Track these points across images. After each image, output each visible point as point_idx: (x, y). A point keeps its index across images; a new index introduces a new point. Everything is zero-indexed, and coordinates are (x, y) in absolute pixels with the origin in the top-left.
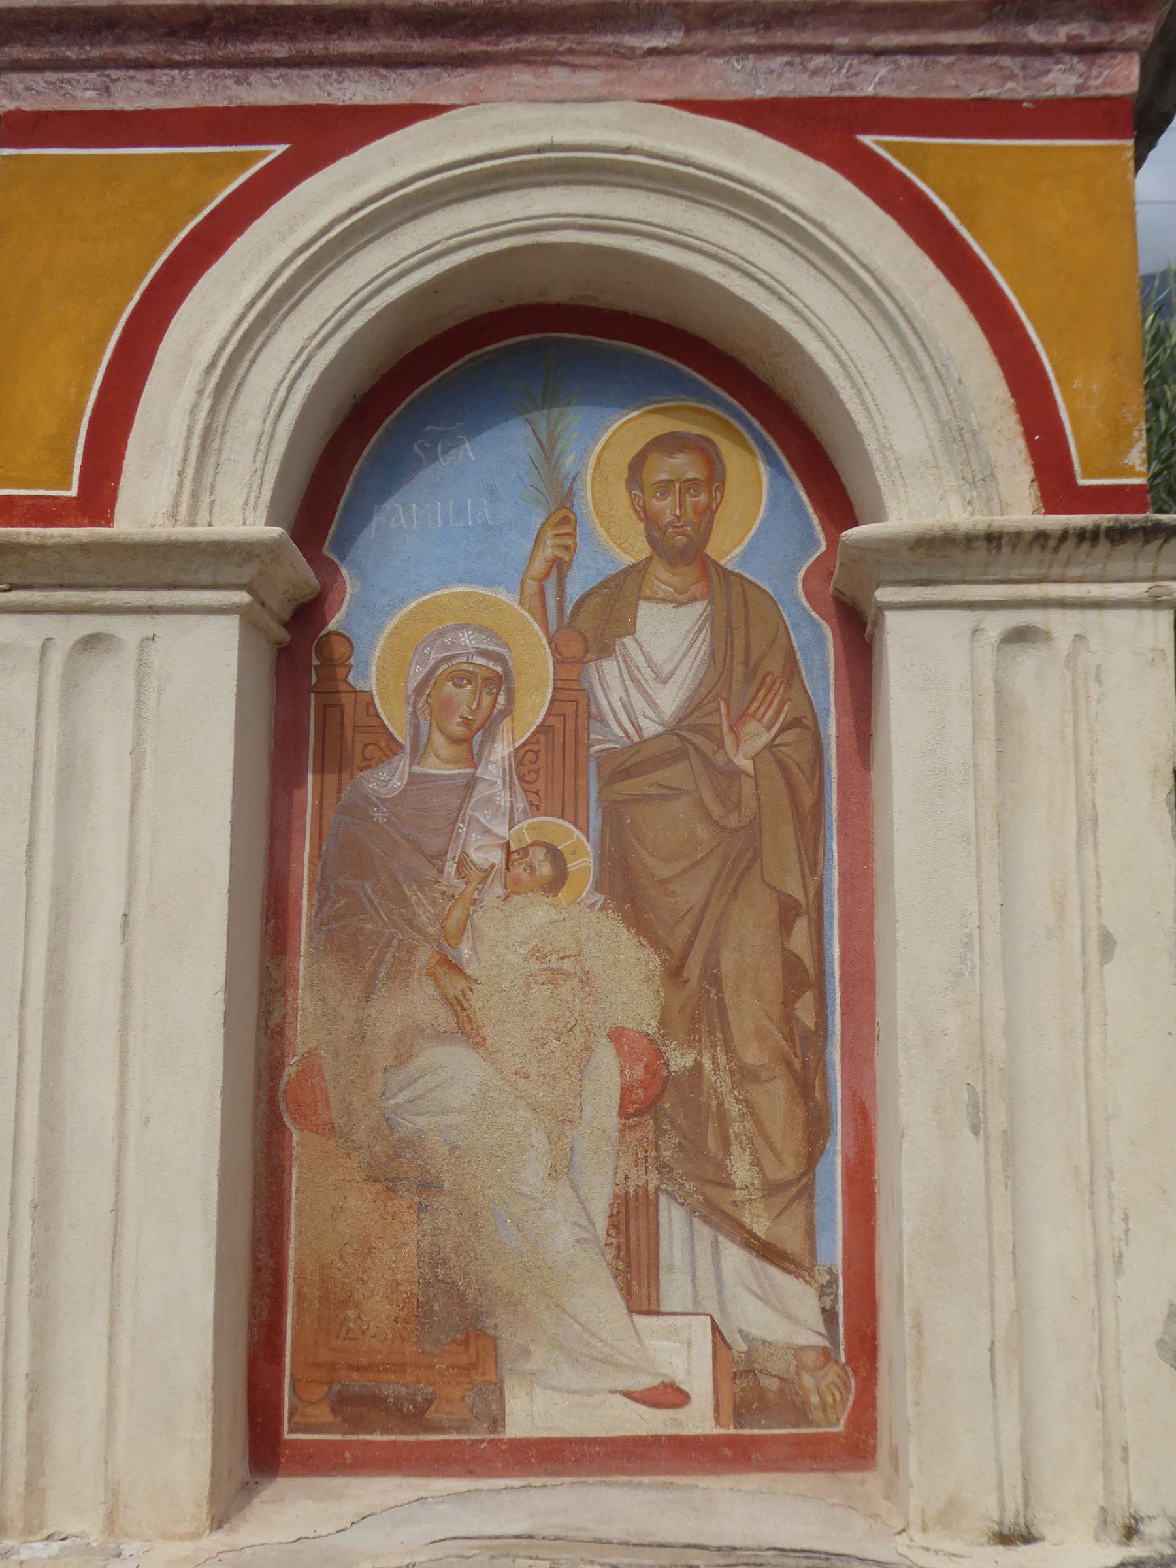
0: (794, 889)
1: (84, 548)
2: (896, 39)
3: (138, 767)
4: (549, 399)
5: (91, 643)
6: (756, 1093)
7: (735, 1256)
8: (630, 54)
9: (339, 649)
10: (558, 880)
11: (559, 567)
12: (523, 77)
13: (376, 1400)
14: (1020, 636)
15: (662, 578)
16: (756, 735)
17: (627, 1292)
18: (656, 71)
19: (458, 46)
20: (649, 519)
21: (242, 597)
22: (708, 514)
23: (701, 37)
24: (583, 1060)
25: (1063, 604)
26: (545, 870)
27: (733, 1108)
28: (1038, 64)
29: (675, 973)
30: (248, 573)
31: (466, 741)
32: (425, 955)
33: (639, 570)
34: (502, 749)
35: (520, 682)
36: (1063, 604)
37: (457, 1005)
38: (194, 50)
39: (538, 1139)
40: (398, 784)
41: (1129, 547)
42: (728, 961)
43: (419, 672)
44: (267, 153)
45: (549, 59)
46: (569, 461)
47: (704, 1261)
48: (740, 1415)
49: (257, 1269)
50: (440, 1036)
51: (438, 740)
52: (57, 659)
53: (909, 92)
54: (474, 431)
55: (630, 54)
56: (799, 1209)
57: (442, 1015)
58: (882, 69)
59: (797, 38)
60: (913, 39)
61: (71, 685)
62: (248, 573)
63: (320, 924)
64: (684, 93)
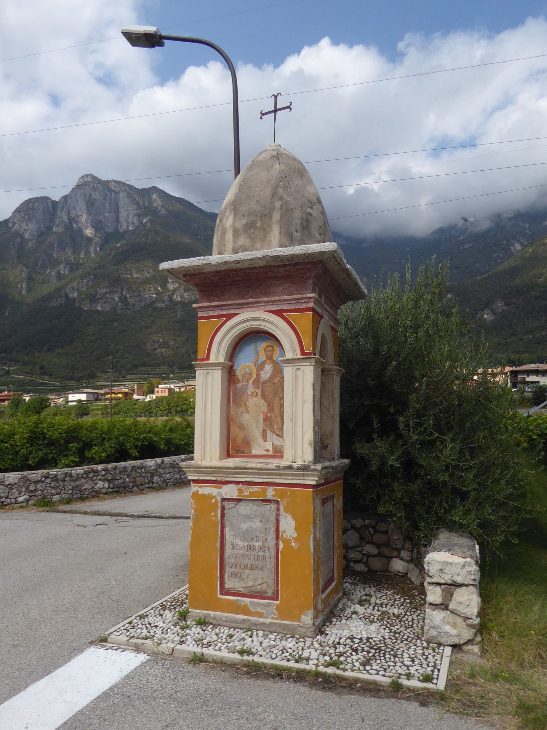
0: (281, 396)
1: (206, 364)
2: (286, 303)
3: (212, 385)
4: (256, 342)
5: (208, 373)
6: (277, 418)
7: (275, 436)
9: (235, 371)
11: (257, 361)
12: (249, 309)
13: (238, 450)
14: (298, 369)
15: (268, 361)
16: (278, 379)
17: (264, 439)
18: (262, 308)
19: (242, 306)
20: (266, 355)
21: (221, 368)
22: (273, 354)
23: (266, 304)
25: (302, 365)
26: (256, 394)
27: (275, 420)
28: (302, 304)
29: (269, 405)
30: (222, 365)
31: (247, 380)
32: (243, 404)
33: (266, 360)
34: (251, 381)
35: (253, 374)
36: (302, 365)
37: (247, 409)
38: (216, 309)
39: (255, 424)
40: (241, 385)
41: (307, 360)
42: (274, 404)
43: (243, 373)
44: (222, 320)
45: (251, 307)
46: (258, 349)
47: (272, 436)
48: (275, 453)
49: (227, 438)
50: (245, 413)
51: (245, 381)
52: (204, 374)
53: (288, 308)
54: (249, 345)
55: (259, 306)
56: (281, 431)
57: (245, 410)
58: (285, 306)
59: (276, 303)
60: (288, 302)
61: (206, 377)
62: (222, 365)
63: (233, 400)
64: (266, 309)
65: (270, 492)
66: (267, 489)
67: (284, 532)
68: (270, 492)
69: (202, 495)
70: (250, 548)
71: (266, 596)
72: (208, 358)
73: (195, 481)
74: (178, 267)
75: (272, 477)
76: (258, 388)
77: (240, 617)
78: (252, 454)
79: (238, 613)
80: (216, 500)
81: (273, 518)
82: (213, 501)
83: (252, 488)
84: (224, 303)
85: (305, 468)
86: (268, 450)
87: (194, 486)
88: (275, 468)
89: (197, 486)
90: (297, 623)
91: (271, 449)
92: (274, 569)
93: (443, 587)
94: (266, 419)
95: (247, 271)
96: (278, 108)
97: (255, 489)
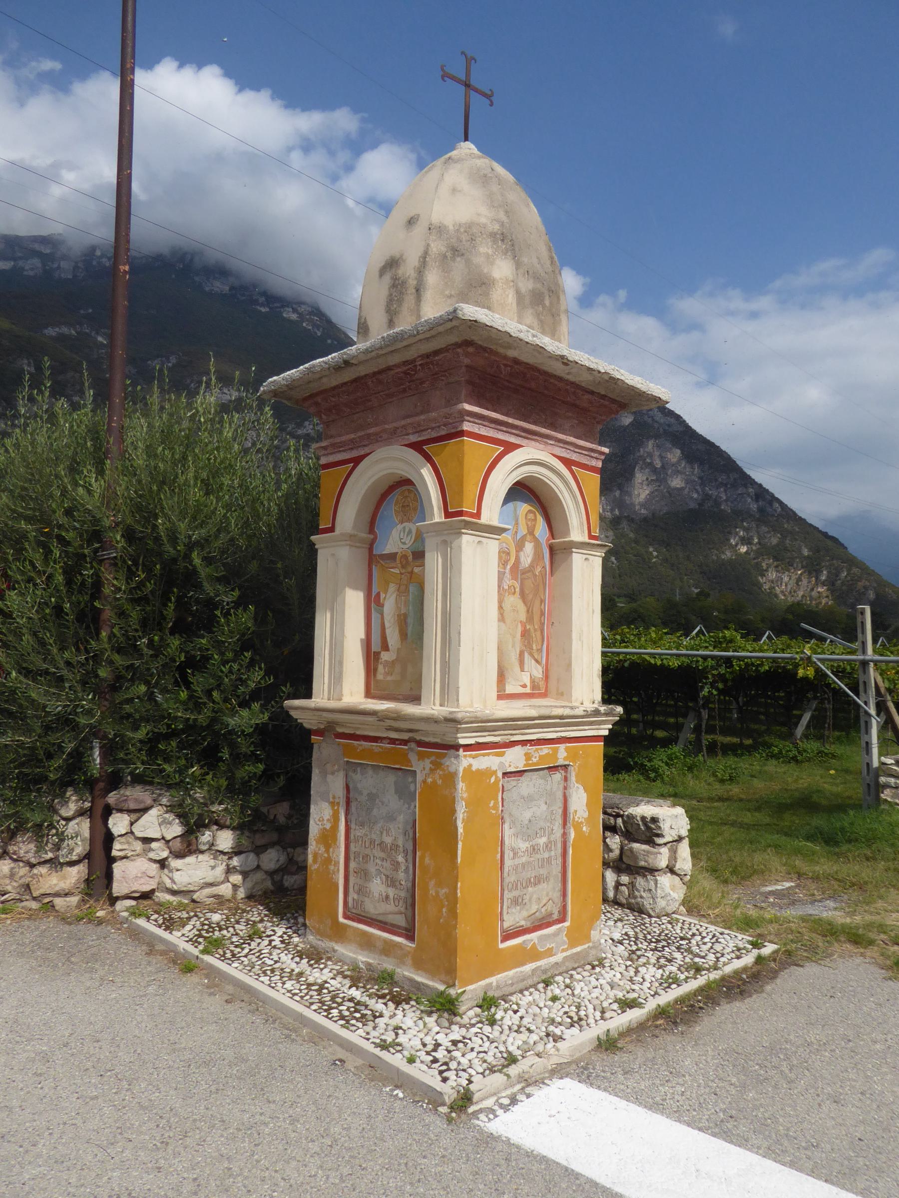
7: (533, 661)
8: (547, 443)
10: (514, 593)
11: (516, 532)
12: (533, 443)
14: (586, 559)
18: (550, 447)
24: (517, 626)
29: (528, 611)
34: (509, 567)
38: (493, 425)
49: (341, 663)
65: (562, 753)
66: (558, 748)
67: (576, 811)
68: (562, 753)
69: (478, 771)
70: (534, 849)
71: (551, 920)
72: (478, 515)
73: (467, 747)
74: (500, 328)
75: (568, 728)
76: (516, 580)
77: (528, 968)
78: (507, 692)
79: (523, 964)
80: (497, 777)
81: (560, 795)
82: (493, 780)
83: (541, 749)
84: (510, 420)
85: (596, 713)
86: (524, 686)
87: (465, 756)
88: (582, 713)
89: (470, 756)
90: (586, 946)
91: (528, 682)
92: (560, 875)
93: (669, 845)
94: (525, 634)
95: (552, 381)
96: (463, 77)
97: (545, 750)
